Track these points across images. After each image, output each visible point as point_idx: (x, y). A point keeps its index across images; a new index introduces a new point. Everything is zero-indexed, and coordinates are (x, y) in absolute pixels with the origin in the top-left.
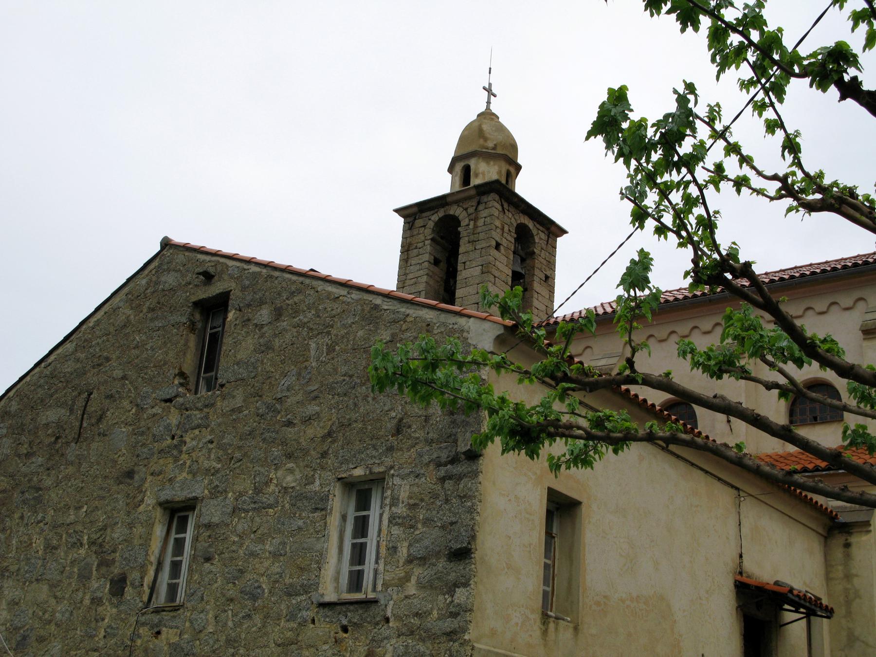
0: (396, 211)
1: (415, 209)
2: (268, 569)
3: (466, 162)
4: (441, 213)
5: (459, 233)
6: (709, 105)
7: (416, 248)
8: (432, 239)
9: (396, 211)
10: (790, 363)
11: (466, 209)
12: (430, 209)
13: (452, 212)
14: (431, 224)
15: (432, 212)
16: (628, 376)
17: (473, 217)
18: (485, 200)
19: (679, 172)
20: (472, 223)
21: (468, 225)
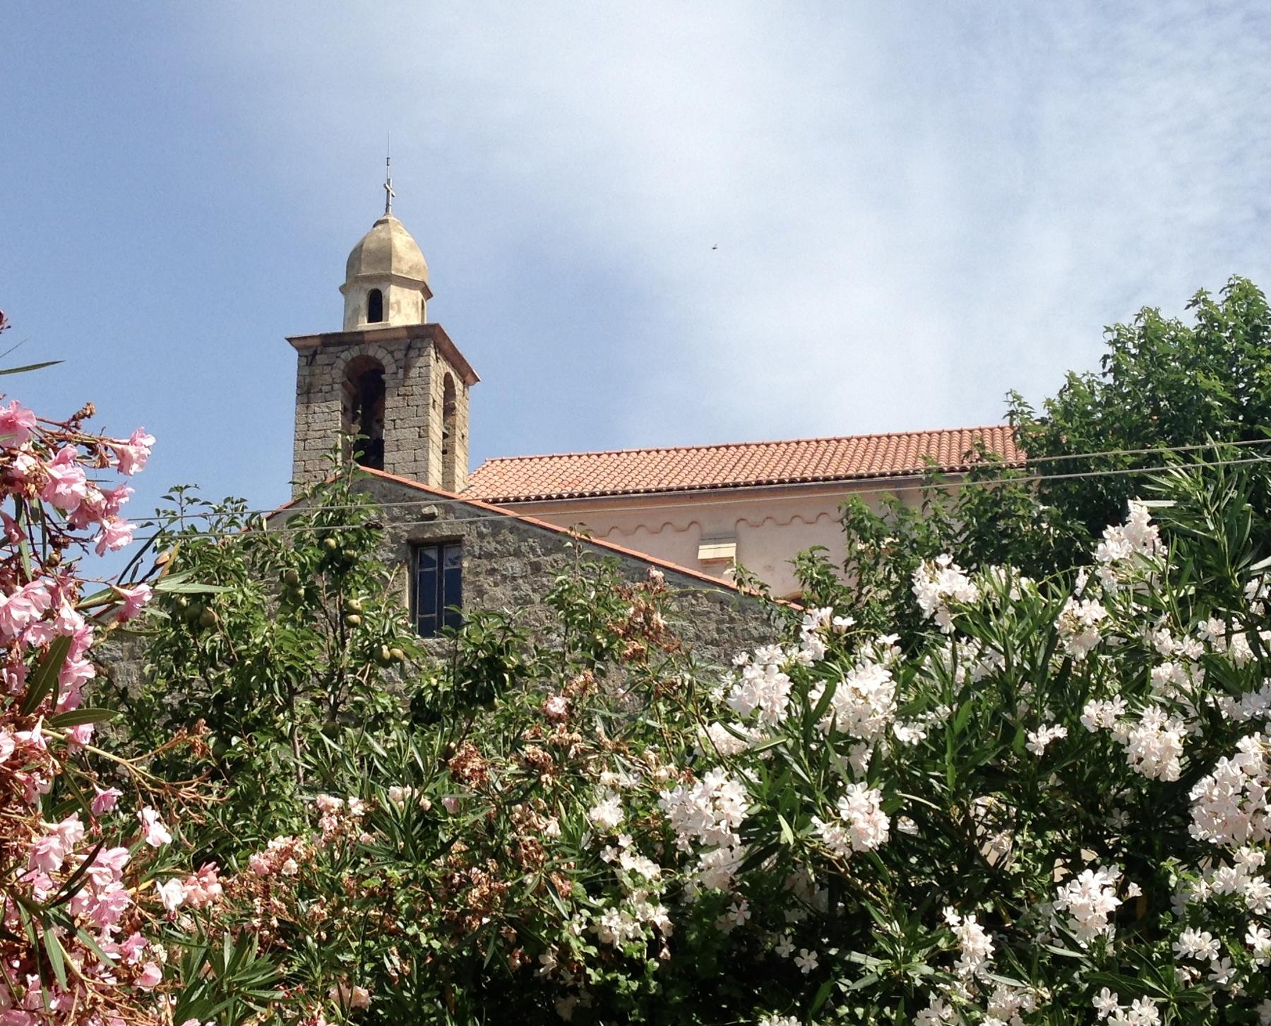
0: (290, 340)
1: (317, 342)
2: (115, 659)
3: (374, 286)
4: (355, 352)
5: (383, 382)
6: (1071, 376)
7: (321, 391)
8: (343, 384)
9: (290, 340)
10: (1086, 577)
11: (391, 353)
12: (340, 343)
13: (371, 353)
14: (341, 364)
15: (340, 348)
16: (437, 837)
17: (403, 364)
18: (419, 345)
19: (492, 708)
20: (401, 371)
21: (396, 373)
